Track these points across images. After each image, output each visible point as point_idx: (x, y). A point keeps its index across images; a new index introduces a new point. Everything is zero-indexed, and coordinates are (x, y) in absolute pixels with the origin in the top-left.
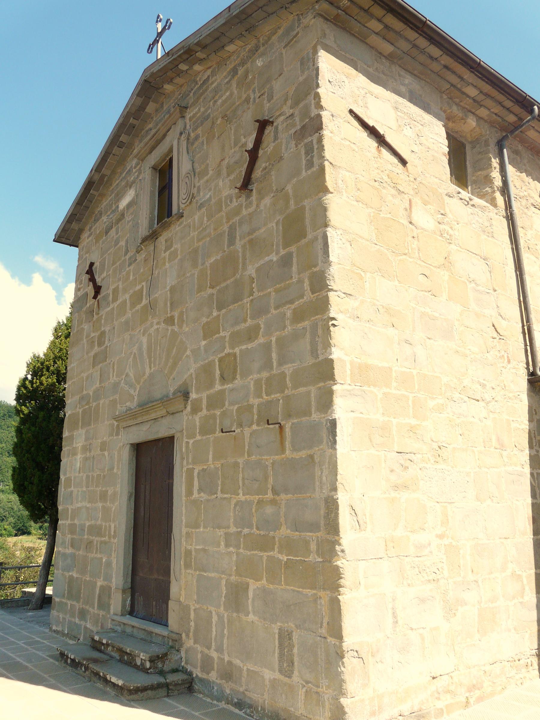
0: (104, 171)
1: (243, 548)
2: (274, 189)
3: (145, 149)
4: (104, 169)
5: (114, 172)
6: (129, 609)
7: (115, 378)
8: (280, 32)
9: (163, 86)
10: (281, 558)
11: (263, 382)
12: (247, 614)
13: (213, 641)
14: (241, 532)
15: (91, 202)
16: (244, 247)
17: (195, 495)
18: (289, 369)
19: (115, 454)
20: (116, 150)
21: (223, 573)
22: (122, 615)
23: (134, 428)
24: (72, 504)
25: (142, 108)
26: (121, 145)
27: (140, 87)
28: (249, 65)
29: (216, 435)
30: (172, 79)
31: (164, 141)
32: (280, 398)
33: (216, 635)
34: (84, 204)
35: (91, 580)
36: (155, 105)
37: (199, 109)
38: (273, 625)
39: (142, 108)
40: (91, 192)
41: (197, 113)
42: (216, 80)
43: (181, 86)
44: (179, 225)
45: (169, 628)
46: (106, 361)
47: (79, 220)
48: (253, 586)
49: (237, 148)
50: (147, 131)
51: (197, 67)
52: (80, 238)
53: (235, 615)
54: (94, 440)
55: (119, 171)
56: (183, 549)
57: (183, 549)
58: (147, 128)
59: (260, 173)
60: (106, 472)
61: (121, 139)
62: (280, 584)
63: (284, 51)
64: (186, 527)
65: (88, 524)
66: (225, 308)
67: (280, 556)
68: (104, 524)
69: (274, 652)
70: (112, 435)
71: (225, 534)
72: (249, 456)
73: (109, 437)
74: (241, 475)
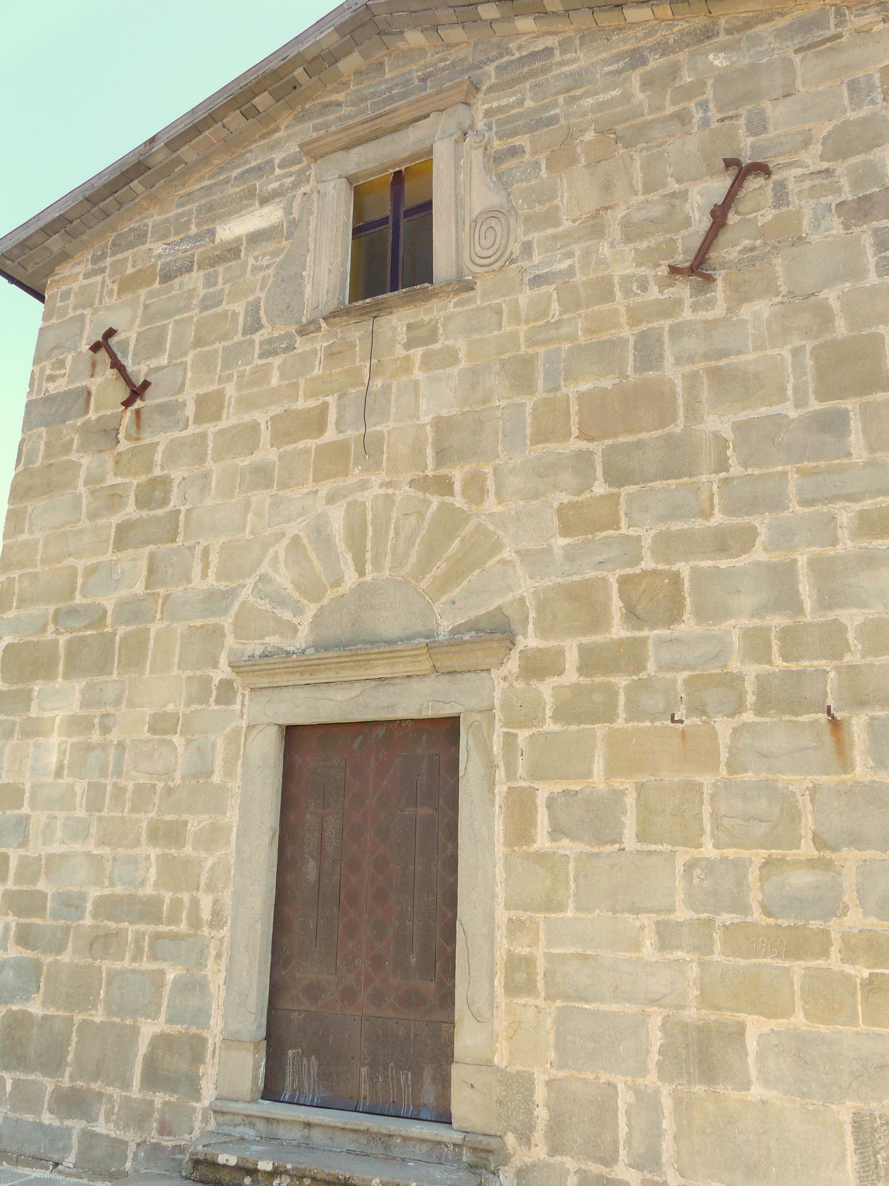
0: (187, 152)
1: (723, 953)
2: (784, 289)
3: (337, 137)
4: (186, 147)
5: (205, 160)
6: (263, 1085)
7: (211, 579)
8: (781, 22)
9: (402, 32)
10: (852, 972)
11: (773, 634)
12: (746, 1085)
13: (621, 1147)
14: (710, 921)
15: (121, 205)
16: (692, 379)
17: (542, 841)
18: (851, 618)
19: (214, 745)
20: (234, 119)
21: (653, 1002)
22: (253, 1101)
23: (301, 694)
24: (24, 844)
25: (332, 57)
26: (250, 113)
27: (348, 15)
28: (682, 56)
29: (615, 726)
30: (435, 27)
31: (395, 135)
32: (828, 669)
33: (630, 1134)
34: (101, 205)
35: (113, 1024)
36: (360, 60)
37: (521, 102)
38: (834, 1107)
39: (332, 57)
40: (131, 185)
41: (510, 107)
42: (575, 61)
43: (450, 46)
44: (456, 305)
45: (454, 1125)
46: (173, 540)
47: (73, 235)
48: (756, 1028)
49: (654, 196)
50: (327, 105)
51: (525, 24)
52: (52, 271)
53: (699, 1089)
54: (123, 708)
55: (216, 162)
56: (500, 955)
57: (500, 955)
58: (327, 99)
59: (735, 254)
60: (178, 781)
61: (255, 101)
62: (852, 1020)
63: (797, 59)
64: (508, 907)
65: (94, 893)
66: (637, 484)
67: (849, 969)
68: (168, 896)
69: (842, 1159)
70: (204, 701)
71: (658, 923)
72: (732, 768)
73: (187, 705)
74: (707, 809)
